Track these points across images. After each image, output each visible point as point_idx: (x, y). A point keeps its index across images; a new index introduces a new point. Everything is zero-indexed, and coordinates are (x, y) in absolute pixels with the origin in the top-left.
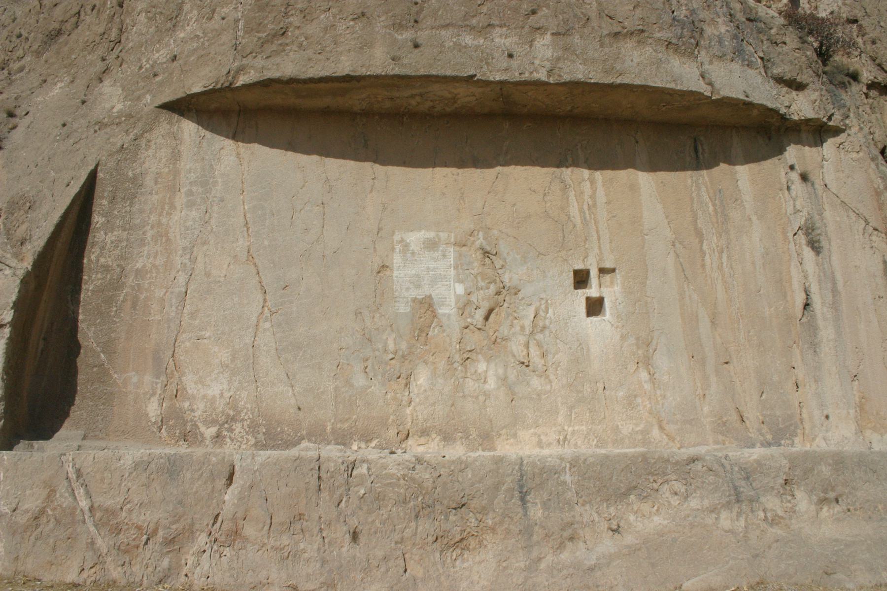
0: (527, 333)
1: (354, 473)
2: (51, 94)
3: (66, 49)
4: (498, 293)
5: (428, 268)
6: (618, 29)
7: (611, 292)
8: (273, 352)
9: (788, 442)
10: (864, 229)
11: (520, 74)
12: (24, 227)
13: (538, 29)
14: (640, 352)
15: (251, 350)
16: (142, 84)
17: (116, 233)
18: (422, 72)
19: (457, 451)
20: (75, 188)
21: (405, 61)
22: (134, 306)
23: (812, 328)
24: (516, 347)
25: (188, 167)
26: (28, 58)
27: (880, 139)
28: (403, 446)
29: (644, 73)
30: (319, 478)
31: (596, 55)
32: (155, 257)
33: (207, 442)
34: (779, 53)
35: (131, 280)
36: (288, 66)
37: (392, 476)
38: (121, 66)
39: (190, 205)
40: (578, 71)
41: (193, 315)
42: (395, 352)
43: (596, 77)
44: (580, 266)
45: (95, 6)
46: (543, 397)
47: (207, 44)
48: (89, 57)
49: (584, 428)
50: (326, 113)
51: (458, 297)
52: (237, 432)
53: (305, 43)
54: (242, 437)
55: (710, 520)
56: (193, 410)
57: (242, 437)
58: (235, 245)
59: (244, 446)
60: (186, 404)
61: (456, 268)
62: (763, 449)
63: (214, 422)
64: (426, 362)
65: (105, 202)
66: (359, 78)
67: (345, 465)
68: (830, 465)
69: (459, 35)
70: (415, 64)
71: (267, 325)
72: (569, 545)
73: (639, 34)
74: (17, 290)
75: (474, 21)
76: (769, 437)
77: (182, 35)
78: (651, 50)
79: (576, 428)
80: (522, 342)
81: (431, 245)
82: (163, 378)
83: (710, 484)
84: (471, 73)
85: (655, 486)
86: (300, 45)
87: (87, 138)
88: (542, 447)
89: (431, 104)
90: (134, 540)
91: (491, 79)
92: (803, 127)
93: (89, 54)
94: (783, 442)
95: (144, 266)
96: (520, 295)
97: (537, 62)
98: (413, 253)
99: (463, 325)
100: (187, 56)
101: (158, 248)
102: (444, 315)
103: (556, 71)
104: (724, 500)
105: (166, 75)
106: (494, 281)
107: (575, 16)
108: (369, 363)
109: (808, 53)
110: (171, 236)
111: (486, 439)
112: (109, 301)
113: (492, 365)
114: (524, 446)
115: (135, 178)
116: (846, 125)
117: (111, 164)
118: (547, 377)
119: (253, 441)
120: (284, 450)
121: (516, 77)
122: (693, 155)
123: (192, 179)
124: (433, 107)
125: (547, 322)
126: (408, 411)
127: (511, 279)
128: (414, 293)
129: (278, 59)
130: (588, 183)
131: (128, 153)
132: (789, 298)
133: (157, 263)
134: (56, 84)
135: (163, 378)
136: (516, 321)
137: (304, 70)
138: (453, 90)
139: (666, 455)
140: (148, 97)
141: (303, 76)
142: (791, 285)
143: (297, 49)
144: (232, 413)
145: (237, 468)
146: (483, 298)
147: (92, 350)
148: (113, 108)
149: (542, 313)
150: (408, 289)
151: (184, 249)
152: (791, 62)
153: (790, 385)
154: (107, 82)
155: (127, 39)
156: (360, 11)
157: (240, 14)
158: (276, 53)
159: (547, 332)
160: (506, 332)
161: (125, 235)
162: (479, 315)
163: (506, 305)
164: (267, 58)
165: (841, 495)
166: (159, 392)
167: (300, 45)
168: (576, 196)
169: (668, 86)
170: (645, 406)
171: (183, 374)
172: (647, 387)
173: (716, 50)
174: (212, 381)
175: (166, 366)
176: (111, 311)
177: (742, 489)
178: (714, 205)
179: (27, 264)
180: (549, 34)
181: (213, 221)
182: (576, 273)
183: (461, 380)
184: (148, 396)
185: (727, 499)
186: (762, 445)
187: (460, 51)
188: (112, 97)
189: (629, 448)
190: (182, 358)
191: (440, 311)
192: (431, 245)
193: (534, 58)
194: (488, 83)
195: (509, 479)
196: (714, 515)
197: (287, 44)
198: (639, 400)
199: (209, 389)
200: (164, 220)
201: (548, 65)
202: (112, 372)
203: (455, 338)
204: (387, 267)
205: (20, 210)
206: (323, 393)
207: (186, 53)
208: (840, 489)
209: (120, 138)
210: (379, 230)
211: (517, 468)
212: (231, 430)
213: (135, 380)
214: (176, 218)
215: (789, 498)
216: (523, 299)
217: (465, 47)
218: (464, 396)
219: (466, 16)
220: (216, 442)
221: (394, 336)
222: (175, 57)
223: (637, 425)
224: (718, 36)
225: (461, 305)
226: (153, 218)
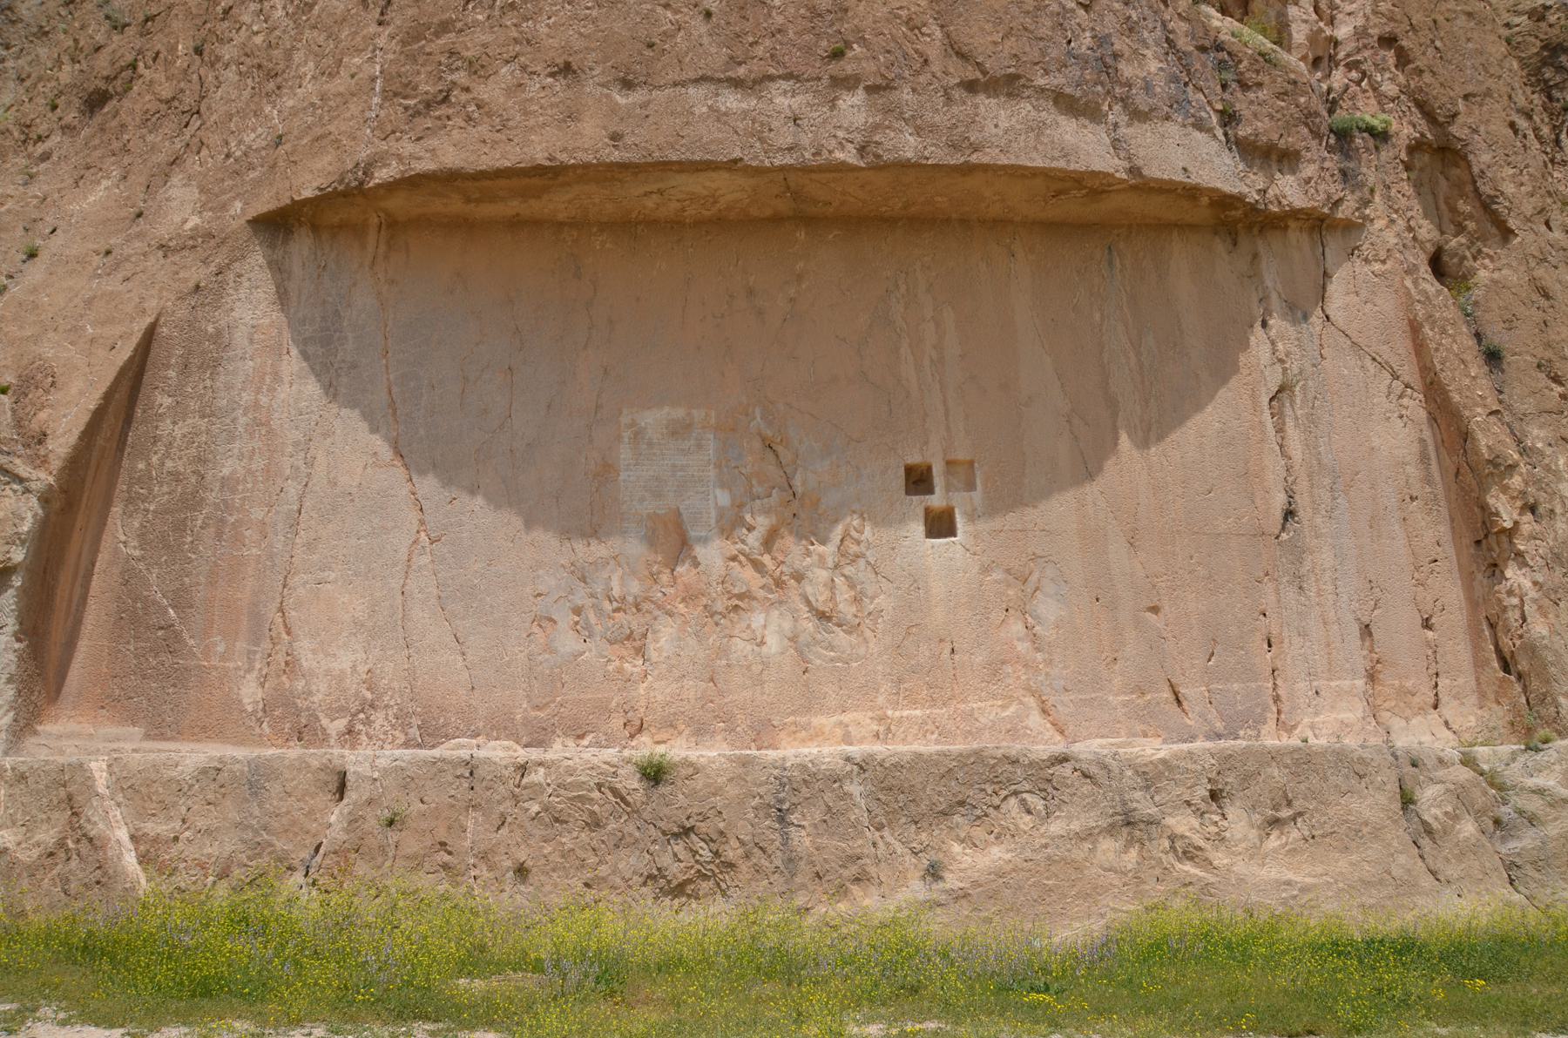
0: (831, 564)
3: (114, 123)
5: (674, 466)
6: (972, 74)
8: (433, 601)
9: (1249, 732)
10: (1390, 386)
12: (43, 415)
13: (846, 83)
15: (399, 598)
17: (189, 421)
20: (125, 352)
22: (219, 535)
23: (1298, 552)
24: (816, 590)
25: (300, 315)
26: (56, 138)
27: (1428, 237)
29: (1014, 145)
31: (937, 118)
32: (251, 459)
33: (332, 742)
34: (1252, 102)
36: (451, 149)
37: (581, 785)
41: (310, 546)
43: (938, 154)
44: (915, 459)
45: (158, 54)
48: (150, 138)
49: (918, 712)
50: (515, 224)
52: (377, 725)
54: (385, 733)
55: (1079, 853)
56: (310, 693)
57: (385, 733)
60: (300, 685)
61: (718, 466)
63: (342, 709)
65: (172, 373)
68: (1286, 767)
69: (717, 95)
70: (648, 139)
71: (426, 559)
72: (855, 889)
73: (1008, 85)
75: (741, 71)
76: (1219, 725)
77: (290, 103)
78: (1029, 108)
79: (905, 713)
81: (678, 430)
85: (996, 801)
86: (469, 119)
90: (194, 883)
91: (767, 163)
94: (1242, 733)
95: (234, 472)
98: (650, 444)
101: (257, 444)
103: (872, 148)
104: (1103, 823)
107: (906, 56)
110: (275, 424)
111: (763, 732)
112: (180, 527)
114: (816, 745)
115: (219, 333)
116: (1365, 218)
119: (402, 738)
123: (307, 334)
127: (804, 483)
129: (433, 142)
132: (1258, 502)
133: (254, 467)
134: (99, 183)
135: (266, 645)
138: (708, 184)
140: (238, 205)
141: (470, 169)
143: (463, 124)
144: (369, 695)
147: (154, 602)
148: (185, 221)
150: (642, 500)
151: (296, 444)
152: (1271, 117)
153: (1259, 643)
154: (176, 179)
155: (209, 108)
156: (560, 61)
157: (378, 67)
161: (203, 424)
165: (1300, 814)
166: (258, 666)
167: (469, 119)
169: (1054, 164)
170: (1018, 678)
172: (1023, 647)
174: (339, 647)
176: (184, 543)
177: (1135, 805)
185: (1110, 820)
186: (1208, 738)
187: (718, 120)
188: (182, 208)
192: (678, 430)
194: (759, 171)
196: (1087, 845)
199: (333, 662)
200: (264, 400)
201: (858, 138)
202: (186, 635)
206: (509, 664)
208: (1298, 804)
210: (598, 407)
212: (368, 722)
213: (221, 648)
214: (282, 396)
215: (1216, 818)
217: (725, 114)
218: (729, 666)
219: (734, 61)
221: (620, 572)
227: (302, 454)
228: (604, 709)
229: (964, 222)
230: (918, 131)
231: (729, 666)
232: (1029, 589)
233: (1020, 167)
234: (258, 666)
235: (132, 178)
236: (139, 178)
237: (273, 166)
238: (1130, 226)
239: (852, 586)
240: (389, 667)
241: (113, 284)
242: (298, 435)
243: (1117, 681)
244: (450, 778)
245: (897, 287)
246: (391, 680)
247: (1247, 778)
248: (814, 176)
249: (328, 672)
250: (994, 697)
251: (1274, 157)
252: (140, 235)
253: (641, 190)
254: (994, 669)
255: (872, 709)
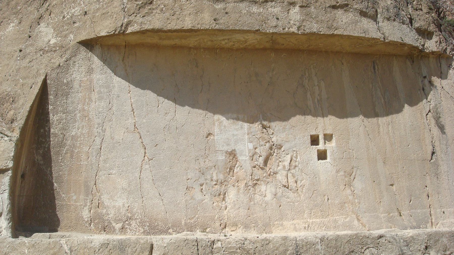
0: (287, 169)
1: (215, 247)
2: (8, 30)
4: (271, 148)
7: (330, 147)
8: (151, 181)
11: (283, 29)
12: (12, 112)
14: (346, 179)
16: (66, 27)
17: (59, 115)
18: (231, 28)
19: (252, 235)
21: (222, 21)
22: (72, 157)
23: (436, 165)
28: (224, 231)
29: (348, 28)
30: (198, 249)
31: (323, 18)
35: (69, 142)
36: (155, 21)
38: (50, 15)
39: (100, 99)
40: (313, 27)
41: (105, 161)
42: (217, 181)
43: (324, 31)
44: (313, 133)
46: (296, 204)
47: (105, 6)
49: (318, 220)
50: (174, 47)
51: (249, 150)
52: (133, 225)
53: (164, 9)
54: (136, 228)
56: (108, 214)
57: (136, 228)
58: (127, 122)
59: (137, 233)
60: (104, 211)
61: (248, 134)
62: (411, 230)
64: (234, 186)
66: (198, 30)
67: (210, 242)
69: (249, 6)
70: (225, 23)
71: (147, 166)
74: (14, 149)
76: (415, 224)
79: (314, 220)
80: (284, 174)
82: (90, 197)
83: (389, 249)
84: (257, 28)
85: (363, 251)
87: (36, 59)
88: (296, 231)
89: (233, 43)
91: (268, 31)
92: (431, 56)
93: (29, 6)
94: (421, 226)
95: (76, 134)
96: (283, 149)
97: (292, 22)
98: (225, 126)
99: (253, 166)
100: (94, 13)
102: (242, 160)
103: (302, 27)
105: (81, 23)
106: (269, 142)
108: (204, 187)
109: (433, 15)
110: (91, 117)
111: (267, 227)
113: (269, 186)
117: (54, 75)
118: (298, 193)
119: (142, 230)
120: (159, 235)
121: (280, 30)
122: (372, 70)
124: (234, 45)
125: (297, 163)
126: (225, 212)
128: (226, 148)
130: (317, 87)
131: (64, 68)
133: (84, 132)
134: (9, 24)
135: (90, 197)
136: (280, 163)
137: (165, 25)
139: (367, 235)
141: (165, 29)
142: (425, 142)
143: (159, 12)
144: (130, 215)
145: (154, 246)
146: (263, 151)
149: (294, 158)
150: (223, 146)
154: (42, 25)
158: (148, 14)
159: (297, 168)
160: (275, 170)
162: (261, 160)
163: (275, 154)
164: (143, 17)
166: (88, 204)
168: (311, 94)
169: (361, 35)
171: (102, 194)
172: (351, 198)
173: (386, 14)
174: (118, 198)
175: (91, 190)
177: (405, 251)
178: (384, 99)
179: (16, 135)
180: (298, 6)
181: (114, 108)
182: (312, 136)
183: (253, 195)
184: (82, 207)
186: (411, 228)
187: (251, 16)
188: (47, 34)
189: (342, 231)
190: (101, 185)
191: (240, 158)
193: (290, 20)
194: (266, 34)
195: (291, 248)
197: (153, 9)
198: (346, 205)
199: (116, 202)
201: (298, 24)
202: (61, 193)
203: (249, 172)
204: (212, 134)
205: (7, 102)
206: (179, 203)
207: (92, 11)
209: (58, 60)
211: (294, 242)
212: (130, 225)
213: (74, 198)
216: (284, 151)
217: (253, 14)
218: (254, 204)
220: (122, 231)
221: (216, 172)
222: (86, 12)
223: (345, 218)
224: (387, 6)
225: (251, 154)
226: (80, 106)
227: (101, 127)
228: (212, 219)
229: (326, 52)
230: (317, 22)
231: (254, 204)
232: (352, 178)
233: (351, 36)
234: (88, 204)
235: (23, 23)
236: (26, 24)
237: (85, 22)
238: (380, 55)
239: (294, 177)
240: (136, 205)
241: (25, 63)
242: (100, 121)
243: (381, 209)
244: (191, 246)
245: (305, 74)
246: (137, 210)
247: (436, 241)
248: (282, 36)
249: (114, 207)
250: (342, 215)
251: (426, 34)
252: (32, 45)
253: (222, 38)
254: (342, 205)
255: (303, 219)
